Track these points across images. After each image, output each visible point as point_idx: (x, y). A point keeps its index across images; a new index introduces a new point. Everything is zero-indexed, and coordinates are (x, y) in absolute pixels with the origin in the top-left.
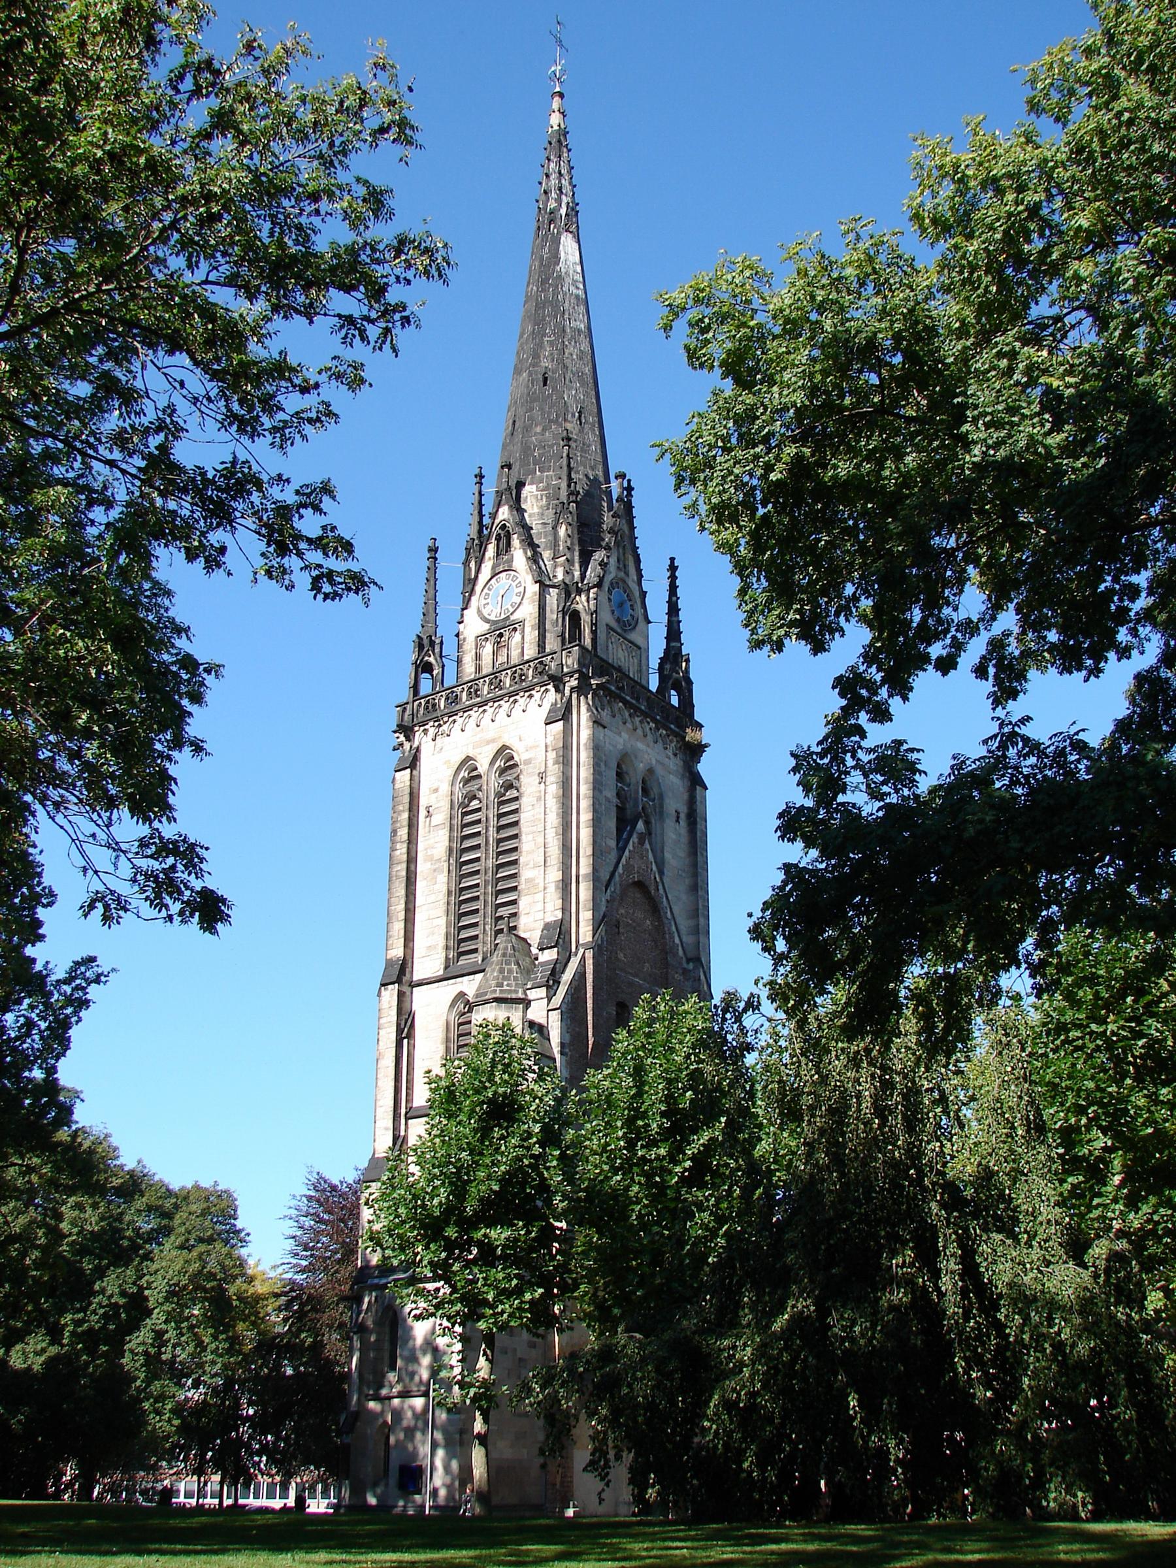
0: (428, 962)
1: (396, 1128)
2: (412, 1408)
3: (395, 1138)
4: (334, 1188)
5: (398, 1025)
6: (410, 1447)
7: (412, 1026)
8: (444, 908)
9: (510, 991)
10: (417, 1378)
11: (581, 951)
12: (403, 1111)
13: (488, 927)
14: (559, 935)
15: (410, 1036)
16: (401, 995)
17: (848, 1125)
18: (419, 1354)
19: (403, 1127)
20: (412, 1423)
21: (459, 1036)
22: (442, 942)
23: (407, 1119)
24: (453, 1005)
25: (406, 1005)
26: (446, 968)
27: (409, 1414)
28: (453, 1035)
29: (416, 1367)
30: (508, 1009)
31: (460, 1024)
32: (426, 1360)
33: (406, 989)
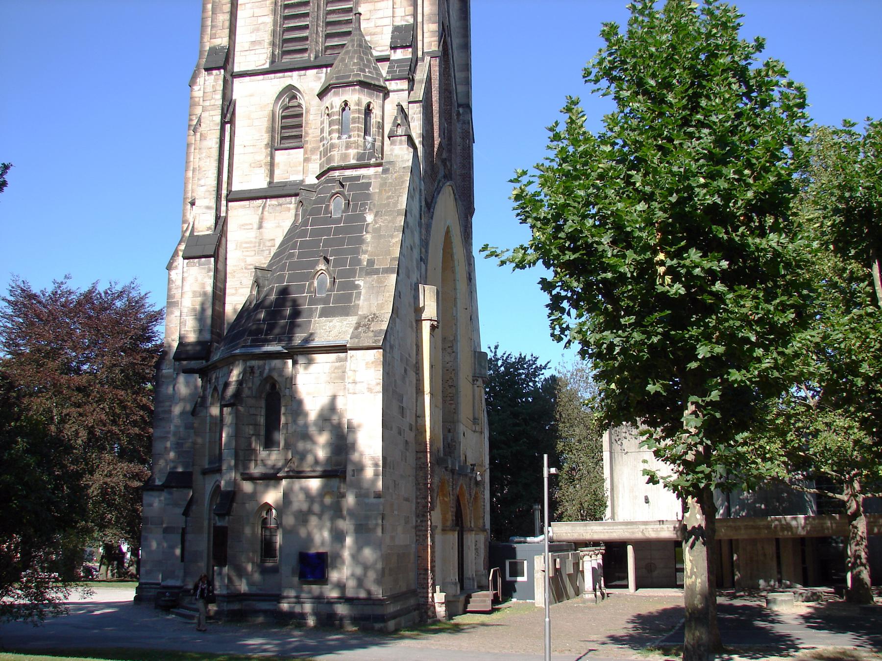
0: (252, 52)
1: (218, 209)
2: (306, 491)
3: (218, 218)
4: (34, 297)
5: (223, 109)
6: (303, 532)
7: (233, 113)
8: (271, 7)
9: (372, 78)
10: (310, 459)
11: (427, 59)
12: (224, 192)
13: (320, 29)
14: (405, 37)
15: (232, 122)
16: (225, 81)
17: (790, 209)
18: (313, 430)
19: (223, 208)
20: (305, 507)
21: (283, 128)
22: (267, 37)
23: (228, 201)
24: (279, 97)
25: (228, 92)
26: (273, 62)
27: (302, 496)
28: (278, 125)
29: (309, 446)
30: (370, 96)
31: (283, 117)
32: (323, 439)
33: (229, 77)
